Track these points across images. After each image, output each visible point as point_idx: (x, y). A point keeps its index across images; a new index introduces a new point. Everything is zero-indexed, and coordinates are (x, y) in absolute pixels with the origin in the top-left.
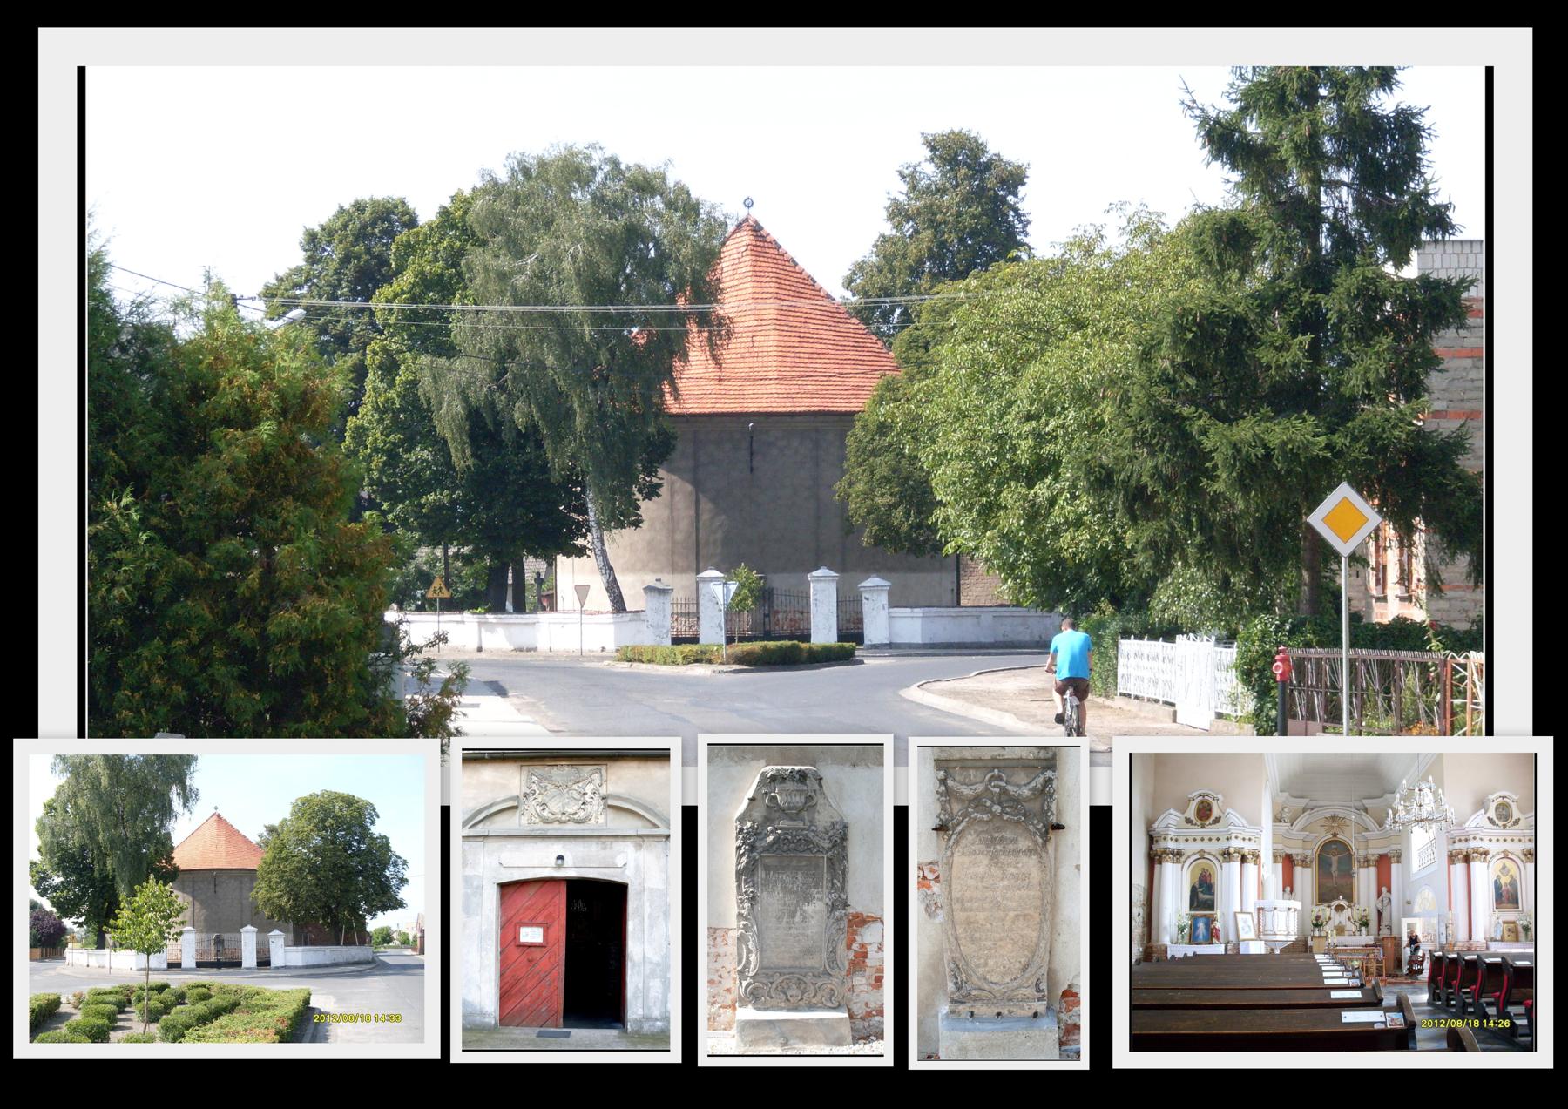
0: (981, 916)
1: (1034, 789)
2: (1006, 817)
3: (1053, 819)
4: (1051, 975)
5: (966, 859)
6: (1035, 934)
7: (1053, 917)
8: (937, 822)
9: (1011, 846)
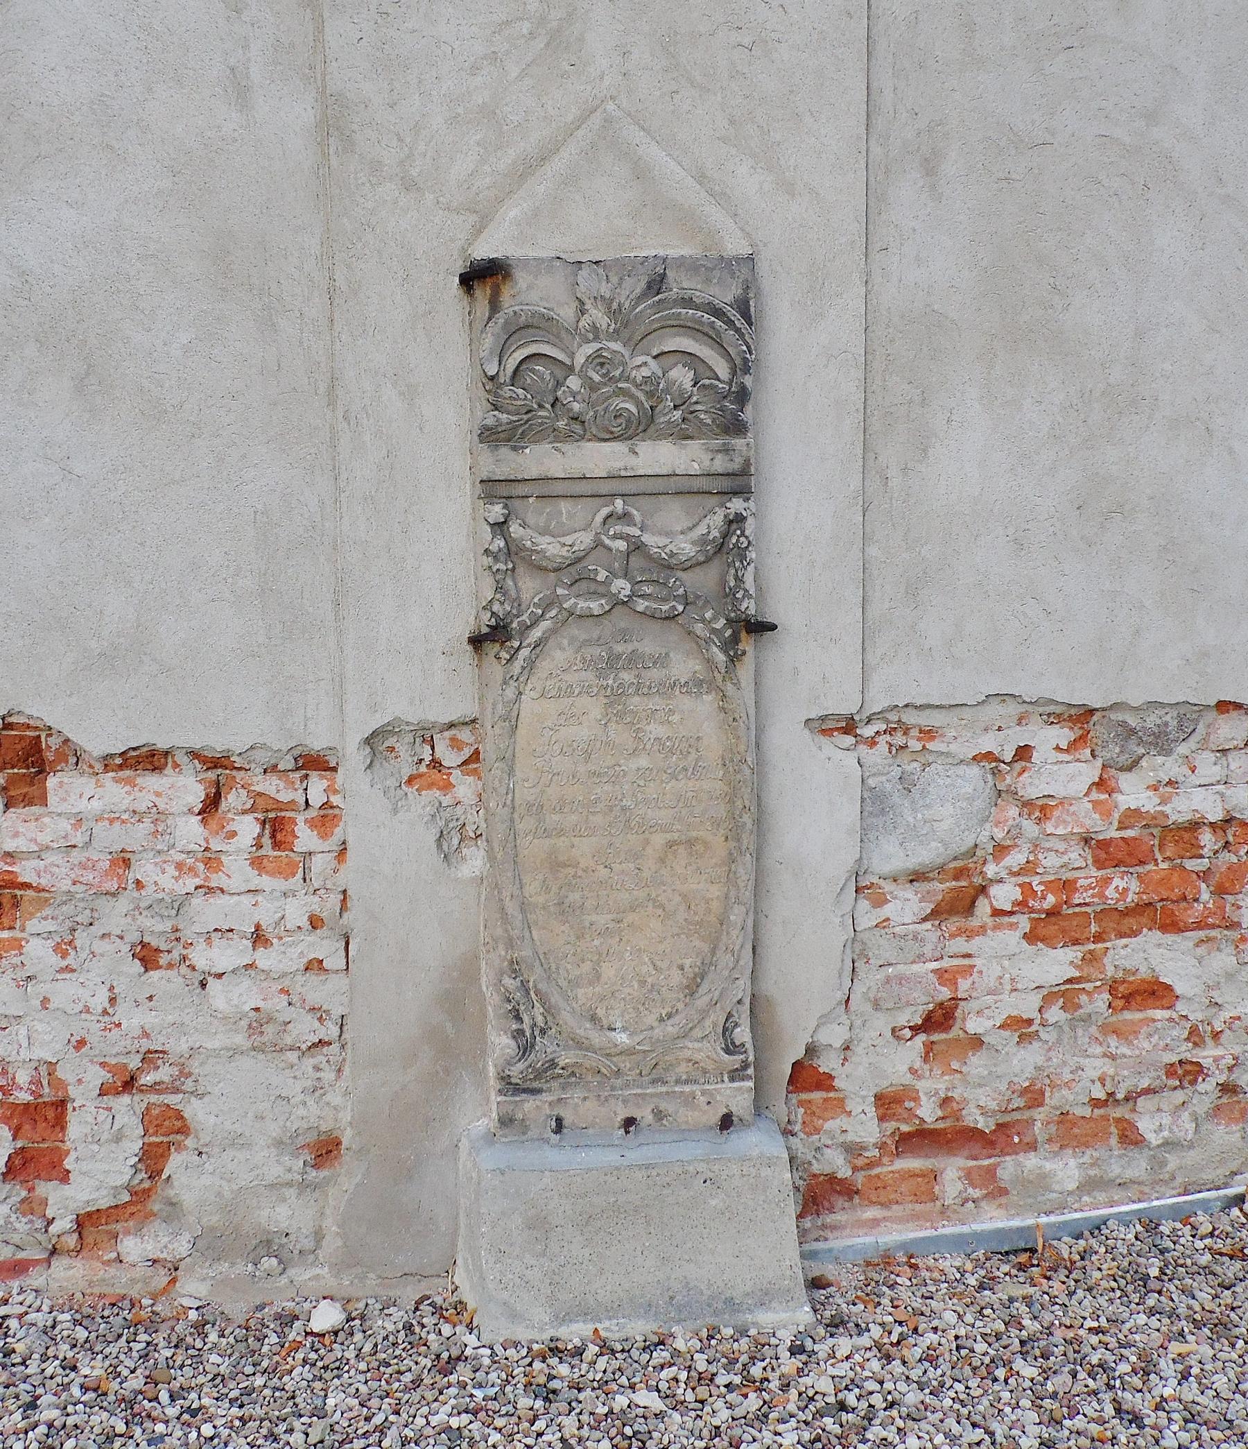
0: (584, 848)
1: (703, 541)
2: (641, 605)
3: (749, 607)
4: (758, 1007)
5: (551, 707)
6: (715, 891)
7: (759, 856)
8: (467, 620)
9: (655, 674)
